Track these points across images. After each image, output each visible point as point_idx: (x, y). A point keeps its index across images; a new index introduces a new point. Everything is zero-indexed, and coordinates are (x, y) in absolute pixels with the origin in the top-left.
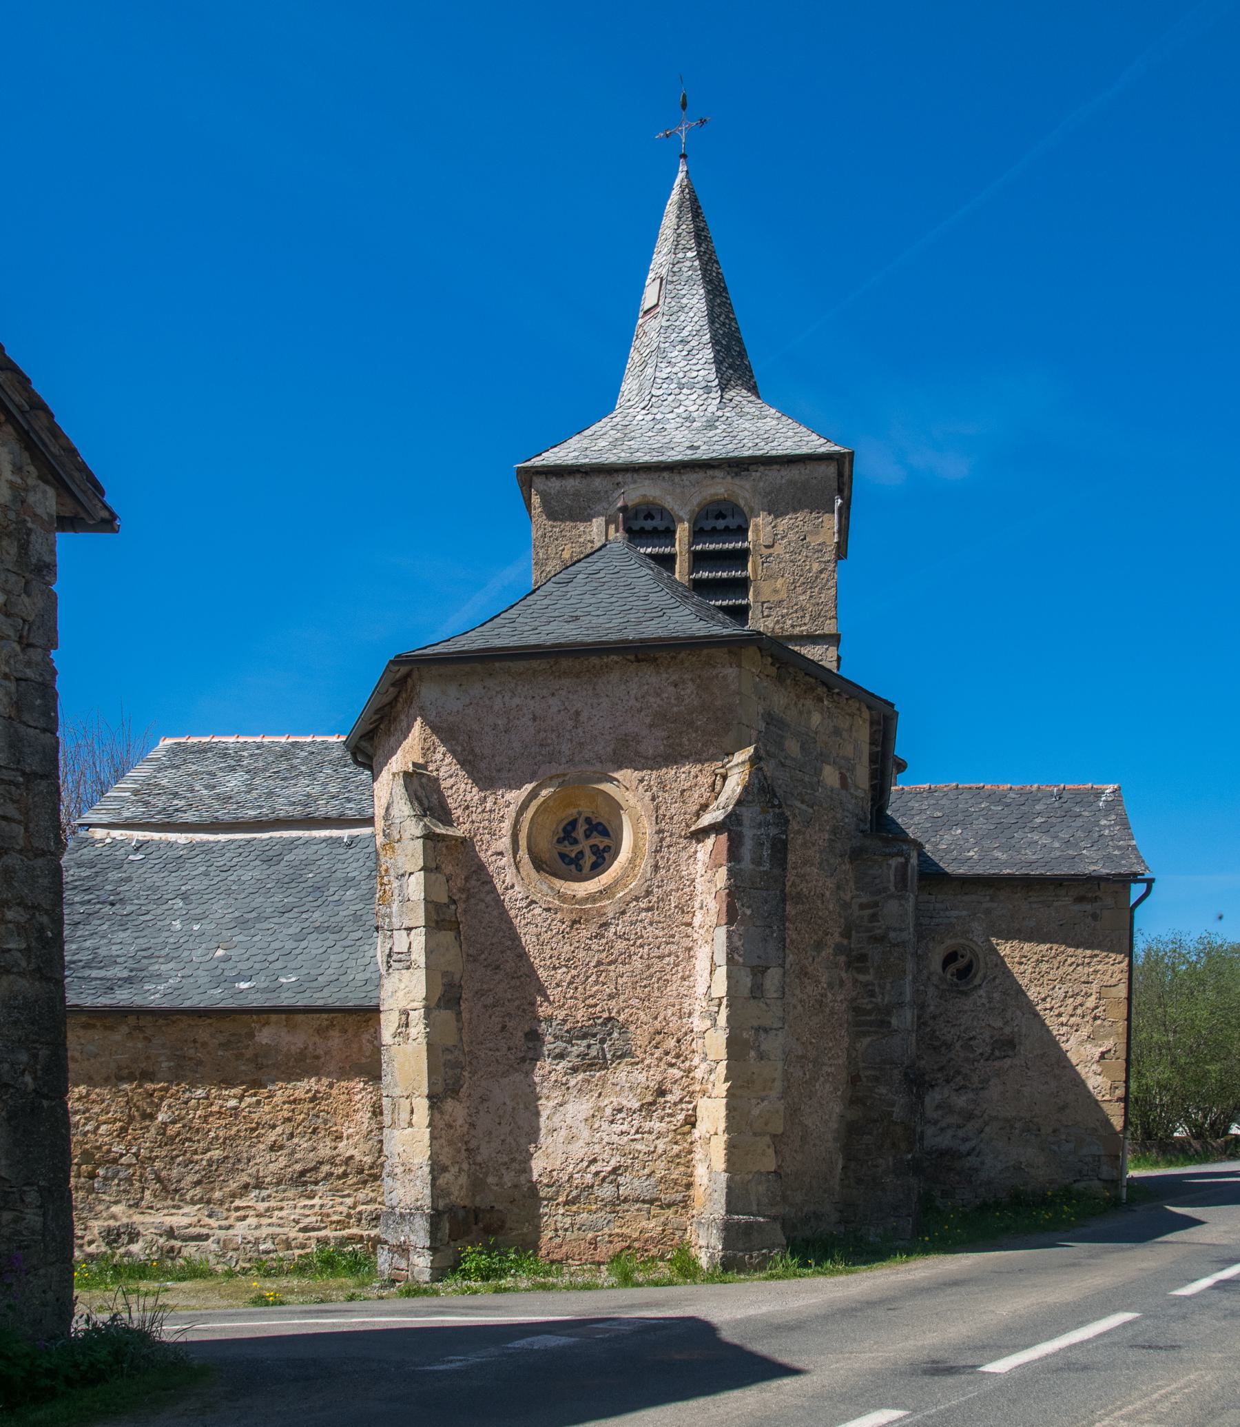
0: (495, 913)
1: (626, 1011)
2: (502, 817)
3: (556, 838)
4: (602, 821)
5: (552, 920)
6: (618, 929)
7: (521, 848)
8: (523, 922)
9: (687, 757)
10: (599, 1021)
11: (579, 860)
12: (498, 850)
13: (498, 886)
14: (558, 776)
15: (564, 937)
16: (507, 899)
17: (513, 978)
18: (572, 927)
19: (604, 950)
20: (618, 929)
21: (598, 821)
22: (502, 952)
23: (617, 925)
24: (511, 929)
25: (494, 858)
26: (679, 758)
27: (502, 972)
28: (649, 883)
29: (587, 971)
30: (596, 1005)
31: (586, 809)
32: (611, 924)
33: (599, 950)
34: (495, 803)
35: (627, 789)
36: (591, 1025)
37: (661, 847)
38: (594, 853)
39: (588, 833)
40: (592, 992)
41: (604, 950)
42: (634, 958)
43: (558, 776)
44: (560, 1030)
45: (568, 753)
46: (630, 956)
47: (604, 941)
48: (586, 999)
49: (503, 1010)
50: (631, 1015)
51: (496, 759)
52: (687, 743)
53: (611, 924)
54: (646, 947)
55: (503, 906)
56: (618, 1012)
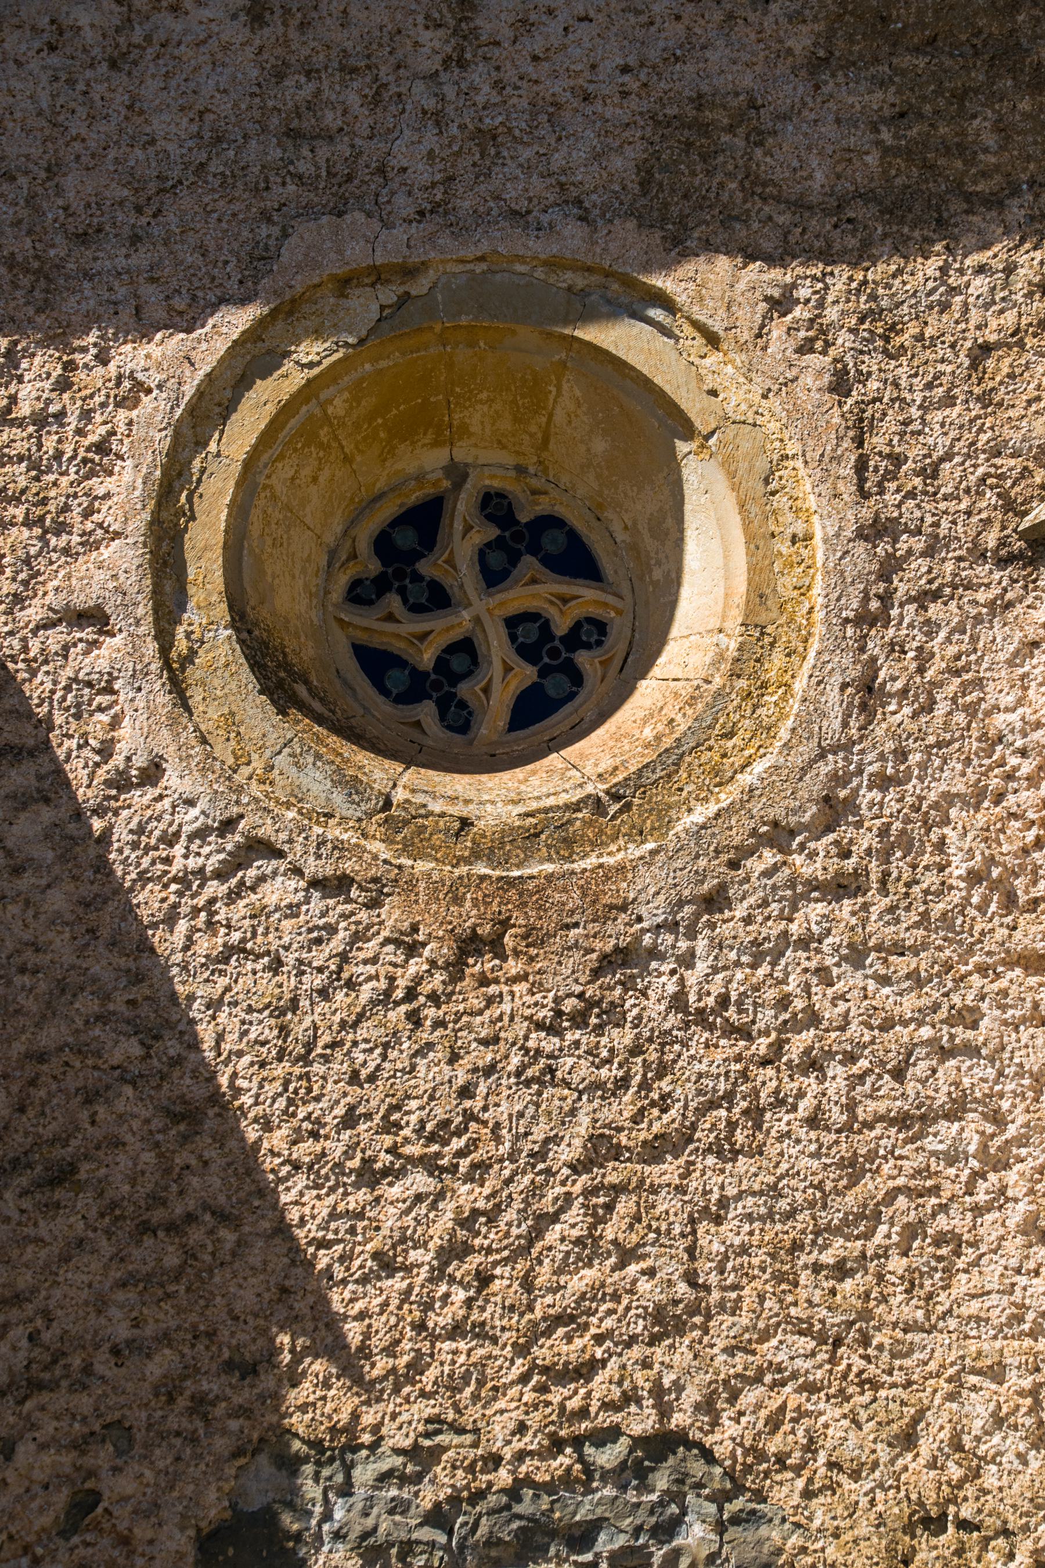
0: (57, 900)
1: (749, 1397)
2: (102, 447)
3: (343, 580)
4: (561, 511)
5: (358, 937)
6: (692, 978)
7: (196, 595)
8: (203, 945)
9: (995, 202)
10: (607, 1457)
11: (456, 679)
12: (80, 601)
13: (77, 771)
14: (378, 275)
15: (415, 1019)
16: (121, 834)
17: (146, 1228)
18: (456, 969)
19: (623, 1083)
20: (692, 978)
21: (543, 506)
22: (90, 1097)
23: (688, 960)
24: (138, 978)
25: (55, 638)
26: (957, 205)
27: (85, 1200)
28: (833, 763)
29: (535, 1191)
30: (585, 1371)
31: (487, 456)
32: (654, 953)
33: (598, 1085)
34: (63, 385)
35: (713, 340)
36: (567, 1480)
37: (886, 599)
38: (527, 653)
39: (496, 559)
40: (565, 1301)
41: (623, 1083)
42: (779, 1121)
43: (378, 275)
44: (399, 1507)
45: (423, 173)
46: (755, 1115)
47: (622, 1038)
48: (535, 1334)
49: (84, 1402)
50: (774, 1423)
51: (70, 182)
52: (990, 140)
53: (654, 953)
54: (836, 1070)
55: (103, 867)
56: (707, 1406)
